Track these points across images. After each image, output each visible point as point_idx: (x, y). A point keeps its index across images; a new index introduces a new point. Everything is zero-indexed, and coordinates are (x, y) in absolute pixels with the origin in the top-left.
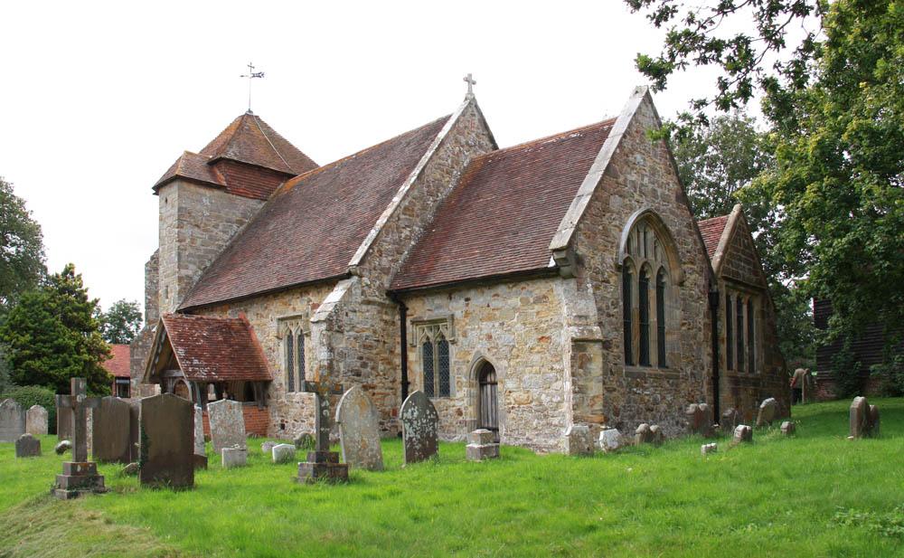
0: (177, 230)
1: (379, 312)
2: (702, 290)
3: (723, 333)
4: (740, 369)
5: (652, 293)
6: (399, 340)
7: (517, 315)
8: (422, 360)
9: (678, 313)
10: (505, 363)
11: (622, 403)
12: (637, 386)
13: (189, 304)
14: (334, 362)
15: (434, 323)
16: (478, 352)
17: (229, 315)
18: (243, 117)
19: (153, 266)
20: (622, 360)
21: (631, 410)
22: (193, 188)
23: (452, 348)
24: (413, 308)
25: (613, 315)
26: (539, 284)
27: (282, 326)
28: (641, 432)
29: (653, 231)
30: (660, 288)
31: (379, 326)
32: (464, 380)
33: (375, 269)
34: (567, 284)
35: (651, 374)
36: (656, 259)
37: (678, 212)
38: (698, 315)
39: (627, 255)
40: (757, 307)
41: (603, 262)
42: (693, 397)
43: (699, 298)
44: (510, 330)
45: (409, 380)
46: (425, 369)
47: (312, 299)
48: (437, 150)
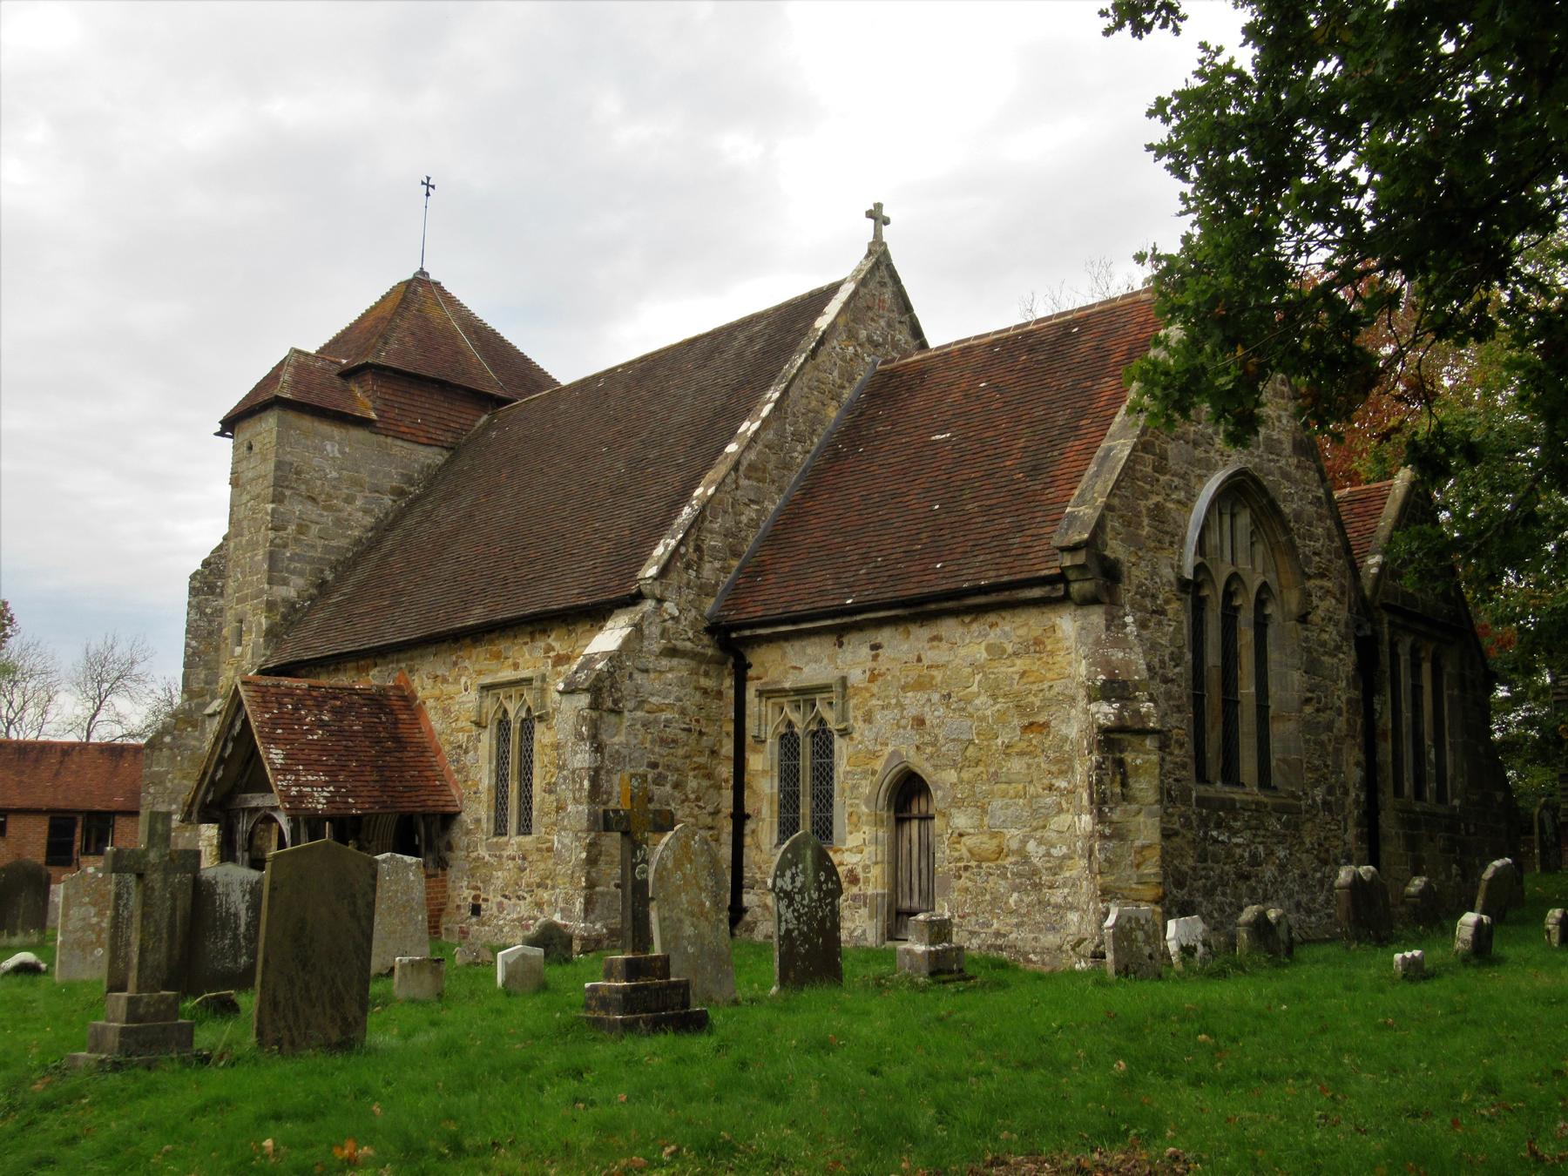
0: (270, 507)
1: (694, 672)
2: (1343, 631)
3: (1385, 721)
4: (1419, 794)
5: (1246, 636)
6: (731, 728)
7: (978, 677)
8: (776, 769)
9: (1296, 677)
10: (951, 776)
11: (1191, 862)
12: (1218, 826)
13: (287, 657)
14: (603, 776)
15: (806, 696)
16: (894, 753)
17: (376, 678)
18: (408, 283)
19: (209, 581)
20: (1189, 773)
21: (1208, 878)
22: (307, 423)
23: (839, 743)
24: (762, 664)
25: (1172, 681)
26: (1024, 616)
27: (490, 705)
28: (1248, 924)
29: (1248, 511)
30: (1261, 625)
31: (692, 700)
32: (864, 809)
33: (688, 586)
34: (1085, 617)
35: (1247, 803)
36: (1254, 569)
37: (1298, 475)
38: (1335, 682)
39: (1199, 559)
40: (1449, 669)
41: (1154, 572)
42: (1327, 851)
43: (1338, 648)
44: (964, 709)
45: (748, 810)
46: (780, 791)
47: (556, 645)
48: (814, 352)
